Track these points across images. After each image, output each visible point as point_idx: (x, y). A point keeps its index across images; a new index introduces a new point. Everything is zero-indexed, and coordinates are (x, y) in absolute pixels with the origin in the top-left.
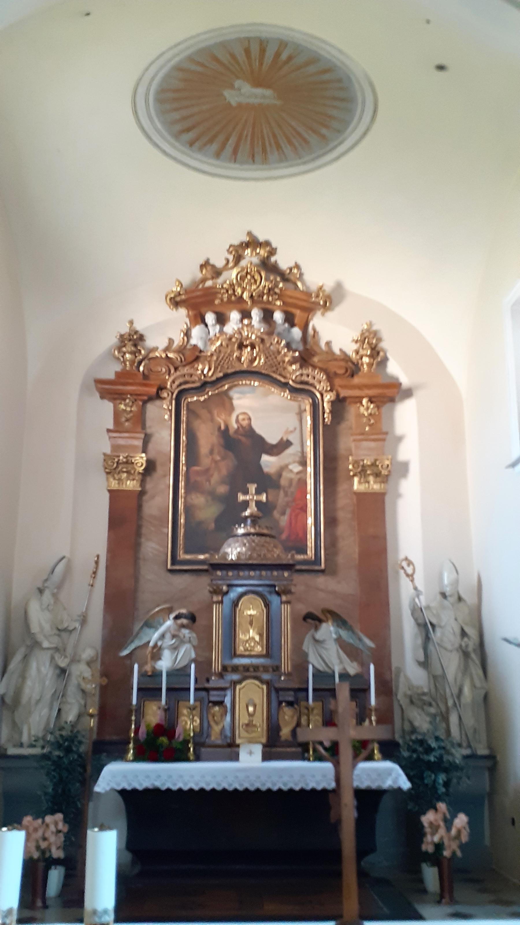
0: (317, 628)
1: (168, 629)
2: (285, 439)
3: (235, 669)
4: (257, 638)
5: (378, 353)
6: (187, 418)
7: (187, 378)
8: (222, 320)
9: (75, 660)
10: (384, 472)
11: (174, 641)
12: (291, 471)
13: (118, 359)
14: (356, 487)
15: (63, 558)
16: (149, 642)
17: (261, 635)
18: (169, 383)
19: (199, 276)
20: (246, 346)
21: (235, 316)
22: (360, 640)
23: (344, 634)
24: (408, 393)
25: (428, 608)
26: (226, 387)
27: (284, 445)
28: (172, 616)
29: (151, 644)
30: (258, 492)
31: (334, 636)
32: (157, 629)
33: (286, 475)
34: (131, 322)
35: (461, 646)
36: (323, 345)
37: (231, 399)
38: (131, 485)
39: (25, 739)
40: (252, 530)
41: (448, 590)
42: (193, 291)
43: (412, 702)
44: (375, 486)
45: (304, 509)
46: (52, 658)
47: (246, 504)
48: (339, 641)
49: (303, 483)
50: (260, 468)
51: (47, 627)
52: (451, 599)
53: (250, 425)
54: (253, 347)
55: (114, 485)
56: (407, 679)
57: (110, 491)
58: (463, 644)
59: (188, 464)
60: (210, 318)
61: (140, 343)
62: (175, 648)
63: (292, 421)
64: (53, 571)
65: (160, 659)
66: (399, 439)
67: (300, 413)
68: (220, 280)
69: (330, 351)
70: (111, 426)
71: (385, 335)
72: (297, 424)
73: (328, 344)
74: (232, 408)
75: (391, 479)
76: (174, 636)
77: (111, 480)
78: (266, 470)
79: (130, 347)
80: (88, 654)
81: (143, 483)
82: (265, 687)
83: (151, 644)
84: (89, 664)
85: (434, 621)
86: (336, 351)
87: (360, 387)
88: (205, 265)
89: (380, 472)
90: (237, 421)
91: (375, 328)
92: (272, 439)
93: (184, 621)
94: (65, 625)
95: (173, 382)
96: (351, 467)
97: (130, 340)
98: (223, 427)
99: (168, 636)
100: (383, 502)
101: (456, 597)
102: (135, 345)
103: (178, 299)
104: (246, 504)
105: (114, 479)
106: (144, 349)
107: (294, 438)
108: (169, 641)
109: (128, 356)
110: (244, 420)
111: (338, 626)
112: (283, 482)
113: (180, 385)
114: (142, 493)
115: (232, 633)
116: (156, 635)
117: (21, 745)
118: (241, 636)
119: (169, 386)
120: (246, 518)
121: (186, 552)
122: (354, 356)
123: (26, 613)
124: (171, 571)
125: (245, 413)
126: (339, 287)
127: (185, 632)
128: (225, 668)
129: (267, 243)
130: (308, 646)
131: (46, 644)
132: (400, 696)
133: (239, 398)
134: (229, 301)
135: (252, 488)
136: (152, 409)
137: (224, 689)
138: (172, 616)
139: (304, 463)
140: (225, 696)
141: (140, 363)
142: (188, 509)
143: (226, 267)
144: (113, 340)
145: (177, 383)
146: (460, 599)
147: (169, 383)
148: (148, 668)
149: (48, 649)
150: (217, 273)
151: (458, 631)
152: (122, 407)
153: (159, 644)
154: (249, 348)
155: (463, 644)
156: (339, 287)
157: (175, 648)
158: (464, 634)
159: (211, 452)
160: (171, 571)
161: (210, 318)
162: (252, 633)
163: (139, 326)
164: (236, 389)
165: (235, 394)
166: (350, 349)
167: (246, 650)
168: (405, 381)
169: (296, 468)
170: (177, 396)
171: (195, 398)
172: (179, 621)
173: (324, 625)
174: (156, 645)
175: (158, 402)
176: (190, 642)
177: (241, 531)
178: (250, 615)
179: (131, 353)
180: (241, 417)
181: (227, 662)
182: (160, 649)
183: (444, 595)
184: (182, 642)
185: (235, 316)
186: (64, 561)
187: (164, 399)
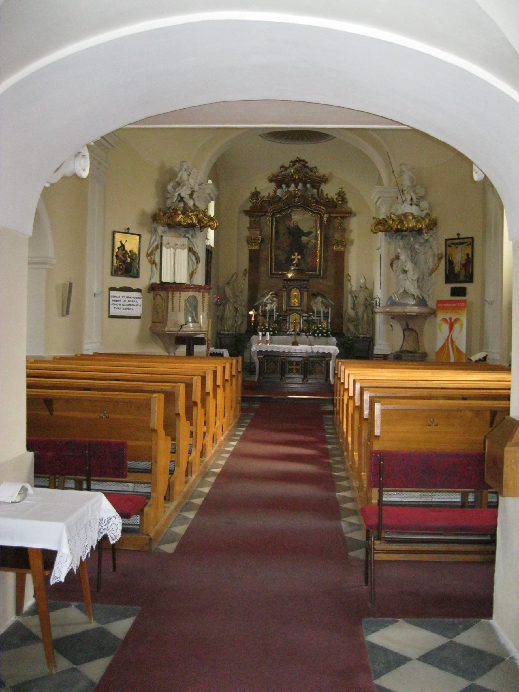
0: (315, 298)
1: (269, 297)
2: (310, 231)
3: (290, 310)
4: (297, 301)
5: (344, 200)
6: (276, 223)
7: (275, 208)
8: (288, 186)
9: (241, 306)
10: (345, 244)
11: (271, 301)
12: (312, 243)
13: (251, 201)
14: (334, 248)
15: (235, 273)
16: (263, 301)
17: (298, 300)
18: (269, 210)
19: (280, 170)
20: (297, 197)
21: (293, 185)
22: (329, 302)
23: (324, 300)
24: (355, 215)
25: (355, 291)
26: (289, 211)
27: (309, 233)
28: (270, 293)
29: (264, 302)
30: (298, 255)
31: (321, 301)
32: (265, 297)
33: (310, 244)
34: (255, 188)
35: (365, 303)
36: (325, 195)
37: (291, 215)
38: (256, 247)
39: (226, 329)
40: (296, 268)
41: (362, 286)
42: (278, 176)
43: (349, 321)
44: (341, 249)
45: (316, 256)
46: (233, 304)
47: (294, 259)
48: (322, 302)
49: (316, 247)
50: (301, 241)
51: (231, 295)
52: (363, 288)
53: (298, 226)
54: (299, 197)
55: (251, 248)
56: (348, 314)
57: (249, 249)
58: (366, 303)
59: (276, 239)
60: (284, 186)
61: (259, 195)
62: (271, 304)
63: (312, 224)
64: (232, 278)
65: (267, 306)
66: (351, 231)
67: (316, 221)
68: (287, 172)
69: (327, 198)
70: (249, 226)
71: (347, 193)
72: (314, 225)
73: (327, 195)
74: (291, 219)
75: (347, 246)
76: (271, 300)
77: (249, 245)
78: (303, 242)
79: (255, 198)
80: (244, 303)
81: (260, 246)
82: (299, 316)
83: (264, 302)
84: (244, 307)
85: (357, 295)
86: (329, 197)
87: (337, 213)
88: (282, 167)
89: (343, 244)
90: (293, 224)
91: (343, 190)
92: (306, 230)
93: (274, 295)
94: (236, 295)
95: (271, 210)
96: (333, 241)
97: (255, 195)
98: (288, 226)
99: (269, 300)
100: (344, 254)
101: (365, 287)
102: (257, 197)
103: (272, 179)
104: (294, 259)
105: (250, 245)
106: (260, 197)
107: (313, 230)
108: (269, 301)
109: (255, 201)
110: (295, 223)
111: (322, 298)
112: (309, 246)
113: (273, 211)
114: (260, 250)
115: (323, 256)
116: (265, 299)
117: (225, 331)
118: (292, 301)
119: (269, 211)
120: (294, 264)
121: (275, 271)
122: (335, 200)
123: (224, 291)
124: (270, 277)
125: (296, 221)
126: (331, 174)
127: (275, 299)
128: (287, 310)
129: (304, 161)
130: (312, 304)
131: (231, 301)
132: (345, 319)
133: (294, 215)
134: (291, 180)
135: (296, 254)
136: (263, 219)
137: (287, 316)
138: (270, 293)
139: (317, 240)
140: (287, 318)
141: (259, 202)
142: (276, 256)
143: (290, 166)
144: (249, 195)
145: (272, 210)
146: (366, 288)
147: (269, 210)
148: (263, 309)
149: (232, 302)
150: (286, 169)
151: (364, 299)
152: (252, 219)
153: (266, 302)
154: (297, 198)
155: (366, 303)
156: (331, 174)
157: (271, 304)
158: (366, 299)
159: (284, 235)
160: (270, 277)
161: (284, 186)
162: (295, 300)
163: (258, 189)
164: (293, 212)
165: (292, 214)
166: (335, 197)
167: (294, 305)
168: (354, 209)
169: (314, 241)
170: (272, 215)
171: (278, 216)
172: (273, 295)
173: (318, 298)
174: (265, 302)
175: (265, 217)
176: (276, 302)
177: (292, 268)
178: (295, 294)
179: (256, 199)
180: (294, 222)
181: (287, 308)
182: (267, 303)
183: (361, 287)
184: (273, 301)
185: (293, 185)
186: (236, 274)
187: (267, 216)
